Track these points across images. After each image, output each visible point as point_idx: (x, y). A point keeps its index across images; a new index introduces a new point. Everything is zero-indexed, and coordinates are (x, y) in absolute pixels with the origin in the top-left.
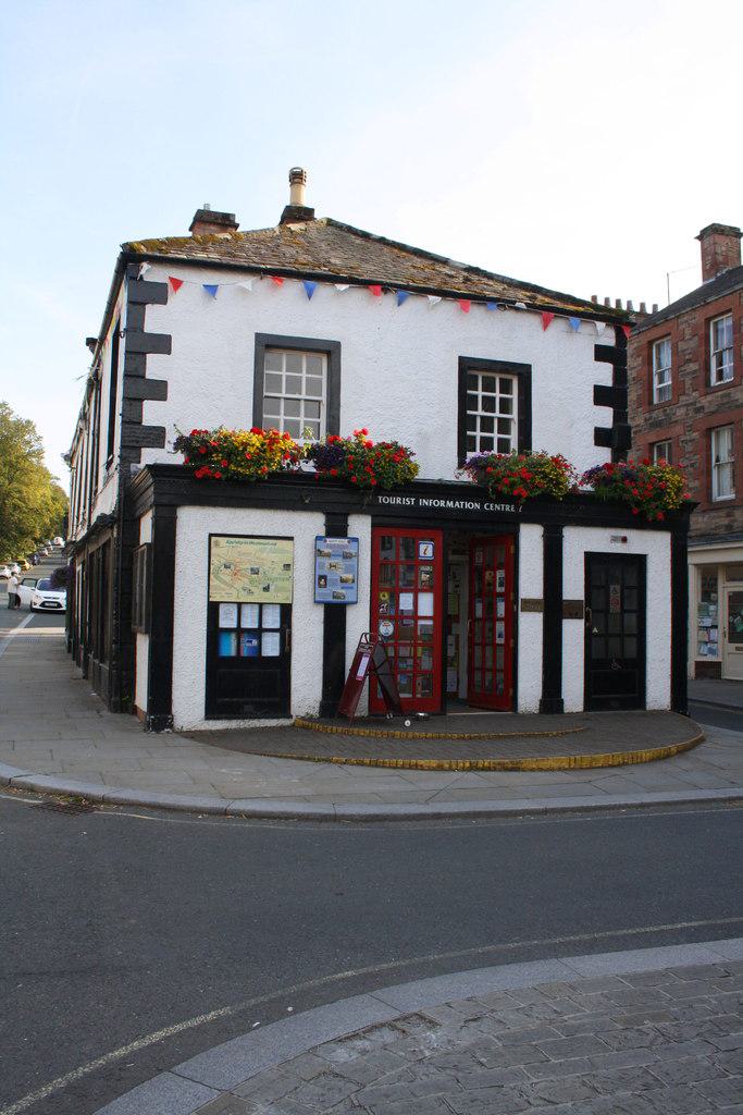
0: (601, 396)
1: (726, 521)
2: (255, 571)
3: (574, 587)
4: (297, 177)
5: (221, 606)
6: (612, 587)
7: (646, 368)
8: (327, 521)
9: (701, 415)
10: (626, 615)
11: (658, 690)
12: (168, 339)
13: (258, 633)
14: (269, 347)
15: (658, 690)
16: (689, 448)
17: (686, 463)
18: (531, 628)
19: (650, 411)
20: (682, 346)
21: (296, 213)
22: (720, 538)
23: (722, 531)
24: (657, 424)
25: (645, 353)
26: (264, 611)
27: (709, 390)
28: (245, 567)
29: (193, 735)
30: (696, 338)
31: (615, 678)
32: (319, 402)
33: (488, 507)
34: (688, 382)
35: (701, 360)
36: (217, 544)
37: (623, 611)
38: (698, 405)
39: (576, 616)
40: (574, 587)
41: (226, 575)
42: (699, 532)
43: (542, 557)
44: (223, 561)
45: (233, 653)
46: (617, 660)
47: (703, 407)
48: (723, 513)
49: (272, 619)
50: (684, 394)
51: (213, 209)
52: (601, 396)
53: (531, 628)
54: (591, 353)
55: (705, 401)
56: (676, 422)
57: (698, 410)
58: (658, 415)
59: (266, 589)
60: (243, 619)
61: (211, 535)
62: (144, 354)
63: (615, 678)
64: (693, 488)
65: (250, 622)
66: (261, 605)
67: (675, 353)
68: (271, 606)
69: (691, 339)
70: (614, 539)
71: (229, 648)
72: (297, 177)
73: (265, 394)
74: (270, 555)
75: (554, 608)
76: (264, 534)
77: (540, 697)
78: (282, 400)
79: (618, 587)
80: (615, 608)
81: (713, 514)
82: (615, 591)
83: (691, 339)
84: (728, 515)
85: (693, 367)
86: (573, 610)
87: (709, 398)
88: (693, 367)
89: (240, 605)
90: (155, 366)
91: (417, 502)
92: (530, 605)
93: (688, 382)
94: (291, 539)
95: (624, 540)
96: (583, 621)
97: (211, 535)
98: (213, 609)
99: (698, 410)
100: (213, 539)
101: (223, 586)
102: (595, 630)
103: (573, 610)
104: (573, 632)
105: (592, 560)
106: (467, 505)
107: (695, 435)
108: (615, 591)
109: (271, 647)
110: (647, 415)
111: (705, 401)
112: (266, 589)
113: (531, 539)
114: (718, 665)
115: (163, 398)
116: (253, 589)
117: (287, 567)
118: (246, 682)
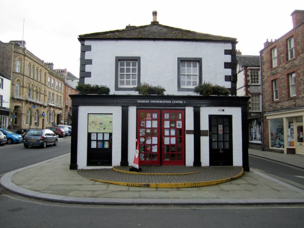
0: (227, 65)
1: (294, 103)
2: (101, 124)
3: (205, 125)
4: (155, 14)
5: (92, 134)
6: (219, 126)
7: (270, 57)
8: (194, 109)
9: (285, 70)
10: (224, 135)
11: (237, 160)
12: (91, 60)
13: (103, 141)
14: (119, 60)
15: (237, 160)
16: (283, 81)
17: (282, 85)
18: (190, 139)
19: (272, 70)
20: (280, 49)
21: (155, 23)
22: (292, 109)
23: (293, 106)
24: (273, 74)
25: (269, 53)
26: (98, 135)
27: (288, 62)
28: (98, 122)
29: (83, 171)
30: (283, 46)
31: (221, 157)
32: (136, 74)
33: (174, 102)
34: (282, 60)
35: (285, 52)
36: (90, 116)
37: (224, 133)
38: (285, 67)
39: (206, 135)
40: (205, 125)
41: (93, 125)
42: (286, 107)
43: (193, 117)
44: (92, 121)
45: (95, 147)
46: (222, 149)
47: (286, 68)
48: (293, 101)
49: (107, 137)
50: (281, 64)
51: (131, 25)
52: (227, 65)
53: (190, 139)
54: (223, 52)
55: (286, 66)
56: (279, 73)
57: (285, 69)
58: (274, 71)
59: (104, 129)
60: (98, 137)
61: (88, 114)
62: (85, 65)
63: (221, 157)
64: (284, 93)
65: (100, 138)
66: (103, 133)
67: (278, 52)
68: (106, 134)
69: (282, 47)
70: (219, 110)
71: (94, 145)
72: (155, 14)
73: (181, 74)
74: (105, 119)
75: (197, 133)
76: (101, 113)
77: (193, 161)
78: (186, 76)
79: (222, 126)
80: (221, 132)
81: (290, 101)
82: (220, 127)
83: (282, 47)
84: (295, 101)
85: (283, 55)
86: (205, 133)
87: (288, 64)
88: (283, 55)
89: (97, 133)
90: (88, 68)
91: (150, 101)
92: (189, 132)
93: (282, 60)
94: (112, 114)
95: (223, 110)
96: (208, 137)
97: (88, 114)
98: (89, 135)
99: (285, 69)
100: (89, 115)
101: (92, 128)
102: (213, 140)
103: (205, 133)
104: (205, 141)
105: (212, 118)
106: (167, 102)
107: (284, 76)
108: (220, 127)
109: (106, 146)
110: (271, 72)
111: (286, 66)
112: (104, 129)
113: (189, 111)
114: (294, 149)
115: (90, 76)
116: (101, 129)
117: (111, 122)
118: (99, 156)
